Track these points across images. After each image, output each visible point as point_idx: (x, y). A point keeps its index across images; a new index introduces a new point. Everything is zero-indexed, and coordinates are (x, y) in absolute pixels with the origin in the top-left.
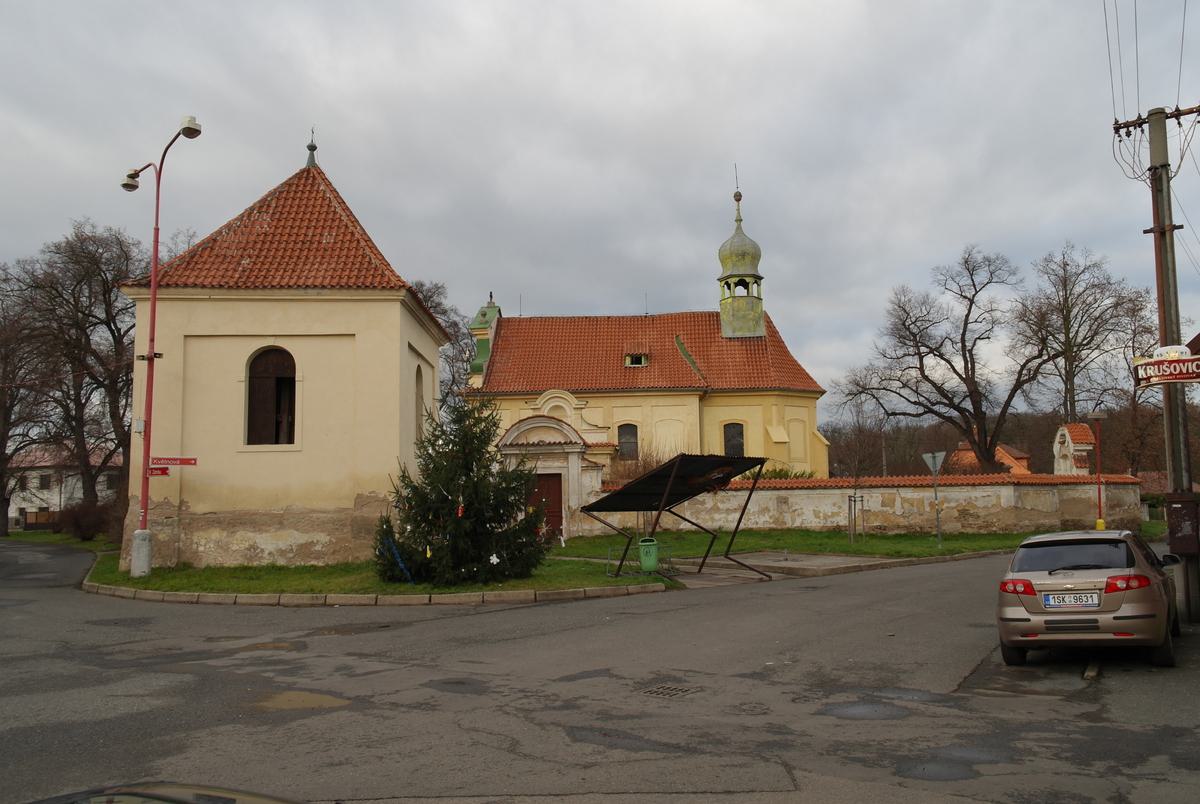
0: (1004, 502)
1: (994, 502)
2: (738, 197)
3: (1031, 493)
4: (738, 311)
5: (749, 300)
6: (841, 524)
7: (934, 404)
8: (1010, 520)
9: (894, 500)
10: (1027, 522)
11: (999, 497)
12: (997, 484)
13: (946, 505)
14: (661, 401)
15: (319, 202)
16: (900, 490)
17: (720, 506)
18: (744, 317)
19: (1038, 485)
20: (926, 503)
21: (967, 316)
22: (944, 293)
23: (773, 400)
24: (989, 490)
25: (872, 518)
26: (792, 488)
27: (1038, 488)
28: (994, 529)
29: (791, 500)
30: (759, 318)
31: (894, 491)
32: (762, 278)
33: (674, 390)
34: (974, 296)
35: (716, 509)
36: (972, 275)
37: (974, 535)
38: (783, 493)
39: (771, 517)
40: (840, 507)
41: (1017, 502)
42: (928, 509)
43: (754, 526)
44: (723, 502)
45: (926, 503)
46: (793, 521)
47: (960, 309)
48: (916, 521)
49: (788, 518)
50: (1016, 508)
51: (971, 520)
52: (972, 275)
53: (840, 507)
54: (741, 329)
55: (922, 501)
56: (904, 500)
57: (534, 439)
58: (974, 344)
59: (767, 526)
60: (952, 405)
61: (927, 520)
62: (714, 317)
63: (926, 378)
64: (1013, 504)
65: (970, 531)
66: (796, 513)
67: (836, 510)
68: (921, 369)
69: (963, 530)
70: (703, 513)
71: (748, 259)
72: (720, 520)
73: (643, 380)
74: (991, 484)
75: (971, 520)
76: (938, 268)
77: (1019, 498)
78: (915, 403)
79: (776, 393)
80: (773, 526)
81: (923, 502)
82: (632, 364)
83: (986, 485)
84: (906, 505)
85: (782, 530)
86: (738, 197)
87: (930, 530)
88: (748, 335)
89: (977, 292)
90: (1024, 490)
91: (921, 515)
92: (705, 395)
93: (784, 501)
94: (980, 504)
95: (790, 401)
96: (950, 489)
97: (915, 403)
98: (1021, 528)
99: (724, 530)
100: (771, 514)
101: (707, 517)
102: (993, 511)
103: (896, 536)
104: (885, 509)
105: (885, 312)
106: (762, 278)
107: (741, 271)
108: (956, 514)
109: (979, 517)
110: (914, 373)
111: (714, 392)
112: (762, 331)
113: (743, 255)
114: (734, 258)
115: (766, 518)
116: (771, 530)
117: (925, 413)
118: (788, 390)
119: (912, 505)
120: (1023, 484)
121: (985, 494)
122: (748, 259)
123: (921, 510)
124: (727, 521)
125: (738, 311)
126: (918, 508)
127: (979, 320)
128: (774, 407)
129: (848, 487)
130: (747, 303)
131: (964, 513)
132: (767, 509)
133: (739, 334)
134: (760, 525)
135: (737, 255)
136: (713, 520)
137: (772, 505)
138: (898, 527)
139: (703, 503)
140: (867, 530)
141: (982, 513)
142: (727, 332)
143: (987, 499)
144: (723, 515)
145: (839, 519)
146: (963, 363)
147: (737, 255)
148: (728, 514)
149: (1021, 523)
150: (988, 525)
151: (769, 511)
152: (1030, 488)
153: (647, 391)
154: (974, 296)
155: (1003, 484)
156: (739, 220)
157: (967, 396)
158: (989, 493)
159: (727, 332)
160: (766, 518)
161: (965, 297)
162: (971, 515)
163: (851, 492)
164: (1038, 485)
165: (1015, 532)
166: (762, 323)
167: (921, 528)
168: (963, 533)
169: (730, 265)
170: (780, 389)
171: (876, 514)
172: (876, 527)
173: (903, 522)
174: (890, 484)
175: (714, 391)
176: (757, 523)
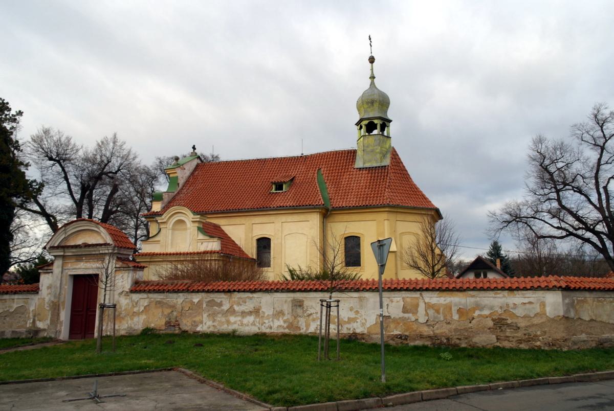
0: (549, 311)
1: (538, 310)
2: (372, 60)
3: (590, 300)
4: (368, 147)
5: (381, 137)
6: (358, 331)
7: (576, 230)
8: (559, 333)
9: (417, 306)
10: (583, 336)
11: (543, 305)
12: (539, 288)
13: (477, 313)
14: (290, 218)
15: (341, 168)
16: (425, 294)
17: (236, 308)
18: (372, 151)
19: (600, 290)
20: (454, 309)
21: (600, 160)
22: (581, 144)
23: (384, 216)
24: (532, 296)
25: (392, 326)
26: (305, 291)
27: (599, 294)
28: (538, 343)
29: (306, 303)
30: (387, 152)
31: (417, 295)
32: (391, 121)
33: (300, 207)
34: (604, 144)
35: (231, 311)
36: (602, 127)
37: (511, 350)
38: (298, 295)
39: (285, 322)
40: (357, 312)
41: (568, 311)
42: (456, 317)
43: (268, 331)
44: (239, 304)
45: (454, 309)
46: (308, 326)
47: (592, 155)
48: (442, 330)
49: (302, 323)
50: (567, 318)
51: (508, 332)
52: (602, 127)
53: (357, 312)
54: (370, 161)
55: (449, 307)
56: (428, 306)
57: (80, 241)
58: (608, 182)
59: (281, 331)
60: (588, 229)
61: (456, 330)
62: (352, 154)
63: (564, 207)
64: (561, 313)
65: (507, 344)
66: (311, 317)
67: (352, 315)
68: (559, 200)
69: (498, 344)
70: (220, 315)
71: (376, 105)
72: (235, 323)
73: (278, 202)
74: (532, 289)
75: (508, 332)
76: (575, 125)
77: (571, 305)
78: (558, 228)
79: (387, 209)
80: (287, 331)
81: (451, 309)
82: (276, 190)
83: (525, 289)
84: (431, 312)
85: (295, 336)
86: (372, 60)
87: (458, 341)
88: (375, 165)
89: (606, 141)
90: (579, 296)
91: (449, 323)
92: (327, 213)
93: (299, 304)
94: (519, 312)
95: (400, 217)
96: (482, 294)
97: (558, 228)
98: (575, 343)
99: (237, 333)
100: (285, 318)
101: (224, 319)
102: (536, 321)
103: (416, 348)
104: (406, 315)
105: (527, 157)
106: (391, 121)
107: (371, 115)
108: (490, 323)
109: (519, 328)
110: (555, 204)
111: (335, 210)
112: (387, 162)
113: (372, 102)
114: (366, 106)
115: (280, 322)
116: (284, 335)
117: (567, 236)
118: (397, 207)
119: (438, 311)
120: (575, 289)
121: (526, 301)
122: (376, 105)
123: (448, 318)
124: (242, 325)
125: (368, 147)
126: (445, 316)
127: (609, 161)
128: (386, 221)
129: (322, 290)
130: (375, 140)
131: (500, 323)
132: (280, 313)
133: (367, 165)
134: (275, 330)
135: (367, 103)
136: (228, 322)
137: (287, 308)
138: (421, 337)
139: (220, 305)
140: (385, 339)
141: (522, 324)
142: (359, 164)
143: (528, 306)
144: (239, 318)
145: (355, 325)
146: (596, 196)
147: (367, 103)
148: (243, 317)
149: (574, 338)
150: (530, 339)
151: (283, 314)
152: (587, 294)
153: (276, 210)
154: (604, 144)
155: (547, 289)
156: (373, 77)
157: (600, 221)
158: (531, 300)
159: (359, 164)
160: (280, 322)
161: (598, 145)
162: (508, 325)
163: (326, 296)
164: (600, 290)
165: (565, 349)
166: (389, 156)
167: (448, 339)
168: (498, 347)
169: (363, 112)
170: (389, 206)
171: (396, 321)
172: (396, 336)
173: (426, 331)
174: (522, 286)
175: (335, 209)
176: (271, 328)
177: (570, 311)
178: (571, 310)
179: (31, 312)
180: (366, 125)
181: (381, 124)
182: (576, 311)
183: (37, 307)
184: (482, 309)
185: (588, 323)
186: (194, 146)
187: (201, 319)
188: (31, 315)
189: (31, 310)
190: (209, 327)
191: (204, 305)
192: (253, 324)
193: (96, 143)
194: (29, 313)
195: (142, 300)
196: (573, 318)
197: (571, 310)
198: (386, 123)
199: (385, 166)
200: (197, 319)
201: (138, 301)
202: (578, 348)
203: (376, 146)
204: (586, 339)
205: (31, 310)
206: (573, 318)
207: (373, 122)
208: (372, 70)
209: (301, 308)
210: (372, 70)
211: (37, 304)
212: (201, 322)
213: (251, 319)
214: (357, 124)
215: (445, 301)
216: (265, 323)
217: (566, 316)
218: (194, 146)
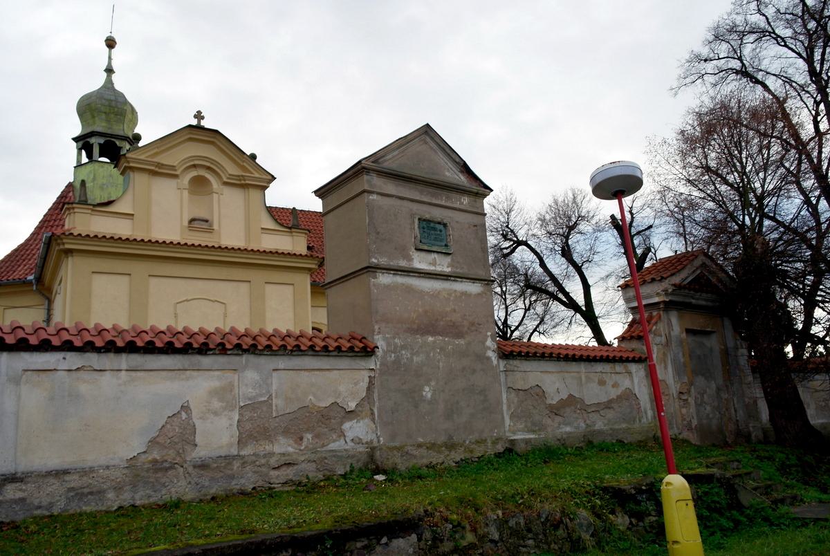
86: (111, 43)
181: (100, 144)
186: (199, 112)
207: (89, 142)
208: (110, 58)
210: (110, 58)
218: (199, 112)
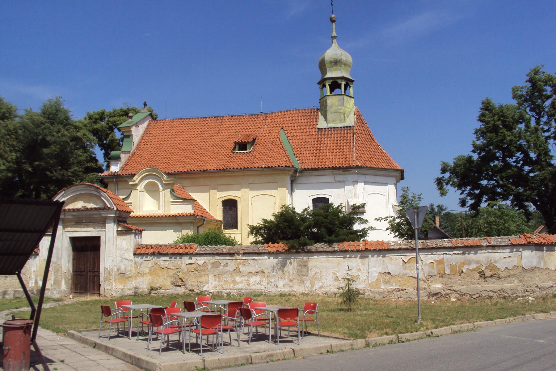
17: (242, 269)
35: (237, 271)
72: (241, 282)
101: (229, 280)
136: (234, 282)
144: (246, 278)
148: (249, 277)
177: (540, 262)
178: (541, 261)
179: (32, 272)
180: (329, 85)
182: (545, 262)
183: (38, 268)
184: (469, 264)
185: (553, 272)
186: (145, 102)
187: (207, 279)
188: (33, 276)
189: (32, 270)
190: (215, 287)
191: (210, 267)
192: (259, 283)
193: (369, 221)
194: (31, 273)
195: (148, 263)
196: (543, 268)
197: (541, 261)
198: (349, 82)
199: (350, 127)
200: (203, 279)
201: (141, 262)
202: (546, 293)
203: (340, 106)
204: (552, 285)
205: (32, 270)
206: (543, 268)
209: (306, 267)
211: (38, 265)
212: (207, 283)
213: (256, 279)
214: (319, 83)
215: (438, 258)
216: (271, 282)
217: (538, 267)
218: (145, 102)
